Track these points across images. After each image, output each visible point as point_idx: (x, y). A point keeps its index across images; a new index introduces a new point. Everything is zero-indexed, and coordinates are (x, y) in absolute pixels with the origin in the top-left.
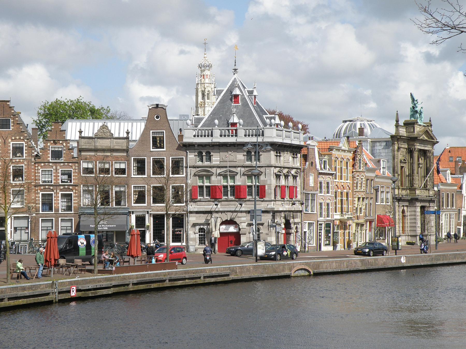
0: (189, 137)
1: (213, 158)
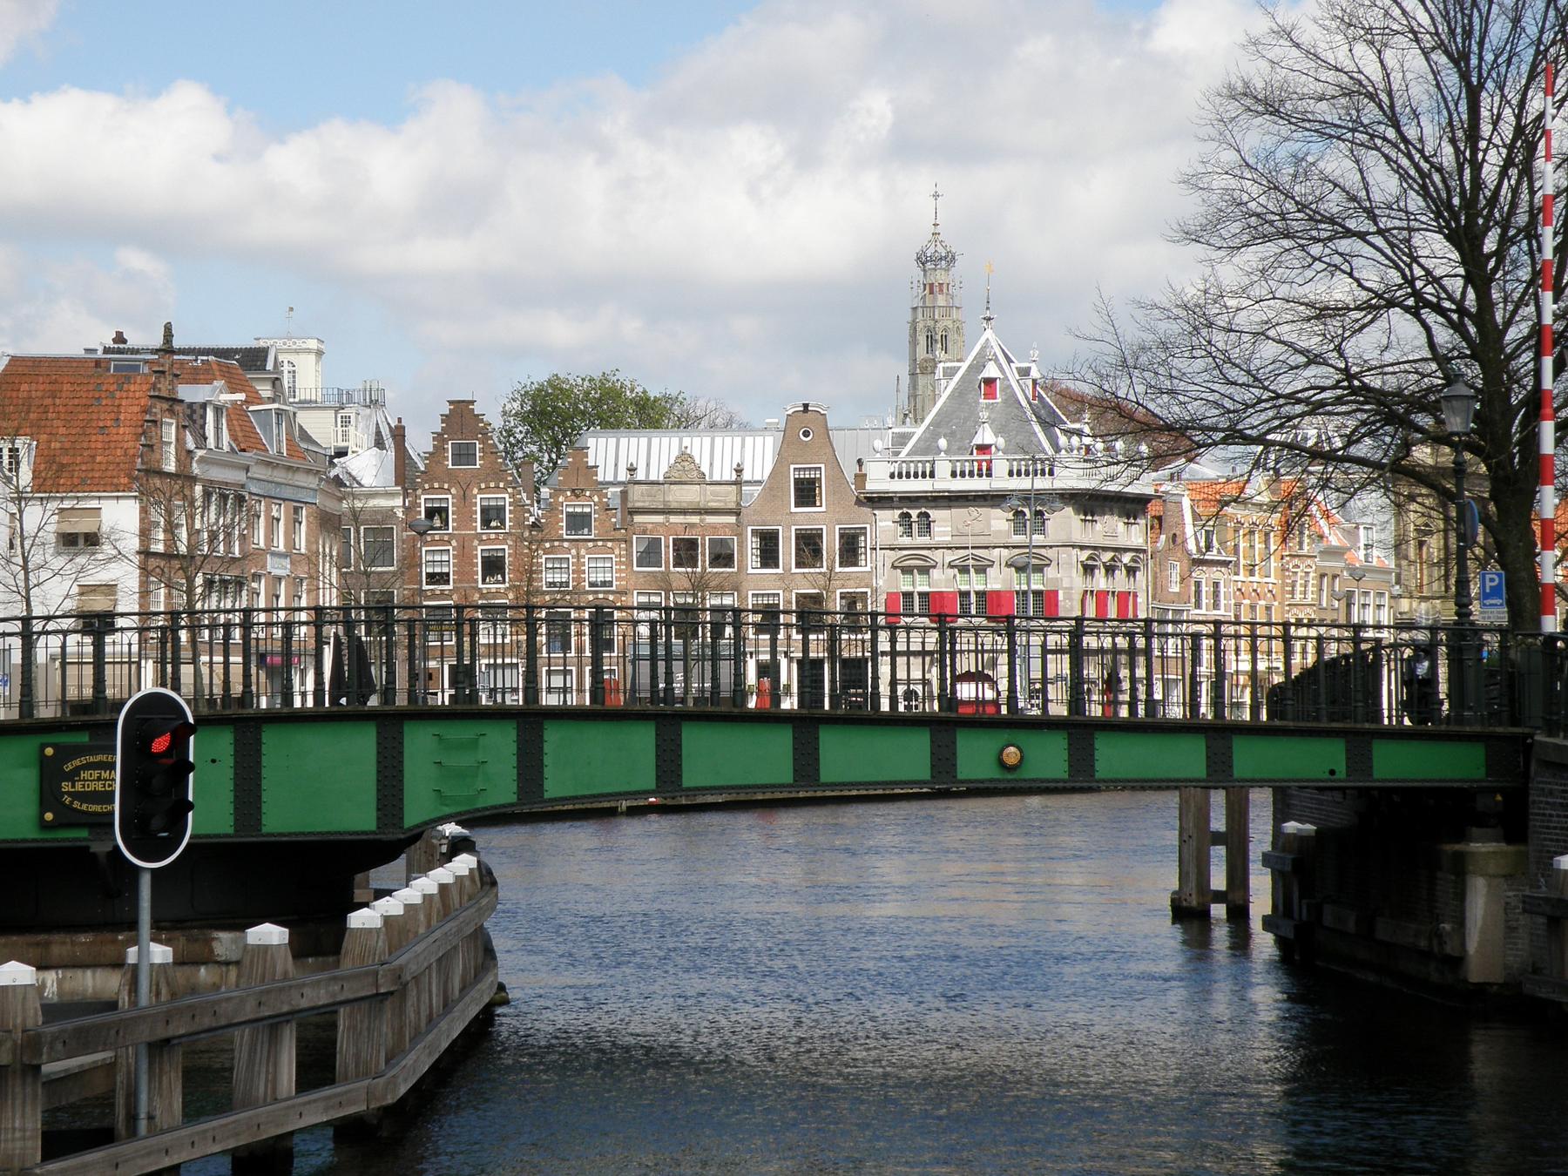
0: (879, 480)
1: (935, 528)
